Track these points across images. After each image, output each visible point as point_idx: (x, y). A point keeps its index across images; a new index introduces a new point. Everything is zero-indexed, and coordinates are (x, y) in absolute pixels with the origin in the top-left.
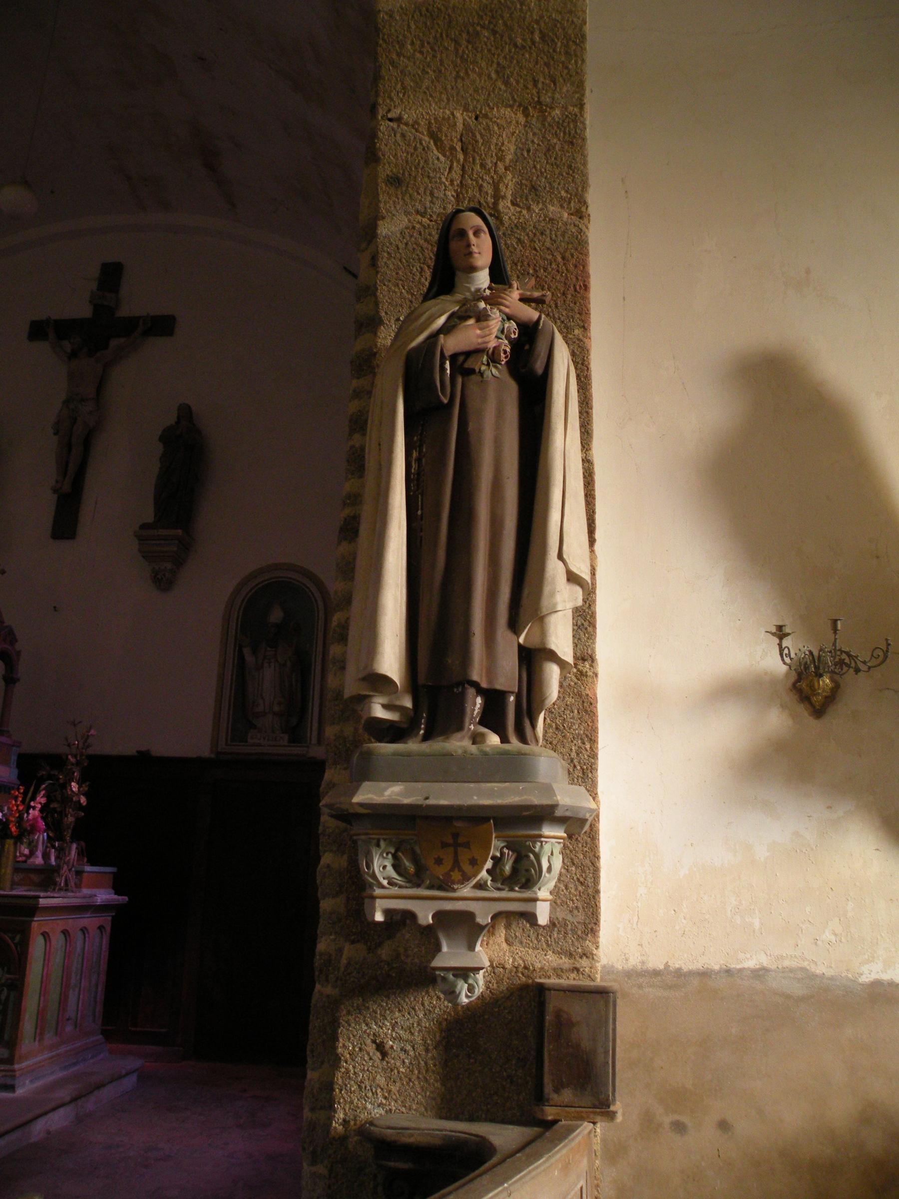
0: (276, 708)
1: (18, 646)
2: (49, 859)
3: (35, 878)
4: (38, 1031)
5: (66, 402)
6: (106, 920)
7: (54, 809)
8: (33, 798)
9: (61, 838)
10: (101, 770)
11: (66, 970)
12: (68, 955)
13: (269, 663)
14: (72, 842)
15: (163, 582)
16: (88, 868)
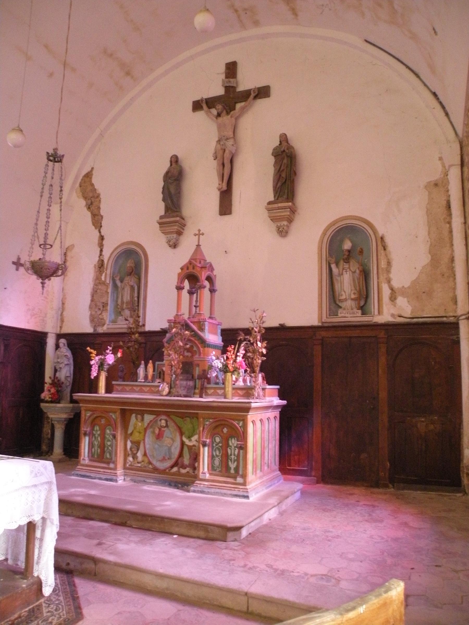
0: (353, 296)
1: (215, 273)
2: (247, 382)
3: (240, 392)
4: (254, 470)
5: (219, 141)
6: (277, 413)
7: (249, 356)
8: (238, 351)
9: (254, 372)
10: (270, 334)
11: (262, 439)
12: (263, 432)
13: (346, 272)
14: (259, 373)
15: (282, 233)
16: (268, 387)
